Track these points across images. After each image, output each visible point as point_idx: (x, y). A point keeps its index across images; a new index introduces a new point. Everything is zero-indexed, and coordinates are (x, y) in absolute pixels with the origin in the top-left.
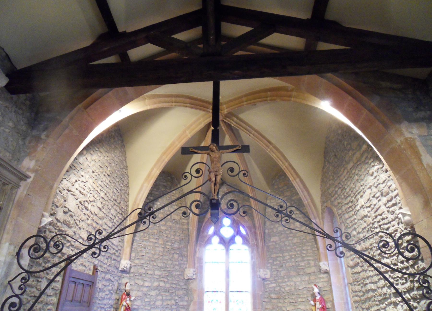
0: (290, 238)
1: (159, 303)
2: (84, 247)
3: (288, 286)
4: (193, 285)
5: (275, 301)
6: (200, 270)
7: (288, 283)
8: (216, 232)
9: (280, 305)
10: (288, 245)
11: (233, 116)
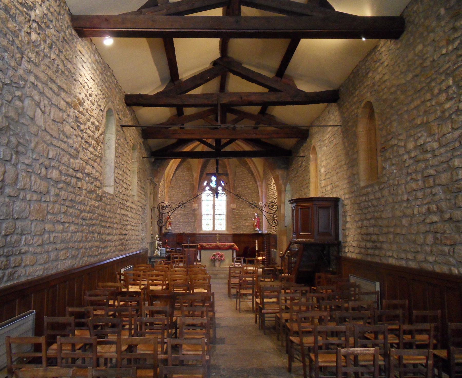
0: (247, 190)
1: (182, 220)
2: (177, 206)
3: (244, 212)
4: (197, 212)
5: (237, 219)
6: (200, 205)
7: (244, 211)
8: (208, 185)
9: (240, 220)
10: (246, 193)
11: (216, 194)
